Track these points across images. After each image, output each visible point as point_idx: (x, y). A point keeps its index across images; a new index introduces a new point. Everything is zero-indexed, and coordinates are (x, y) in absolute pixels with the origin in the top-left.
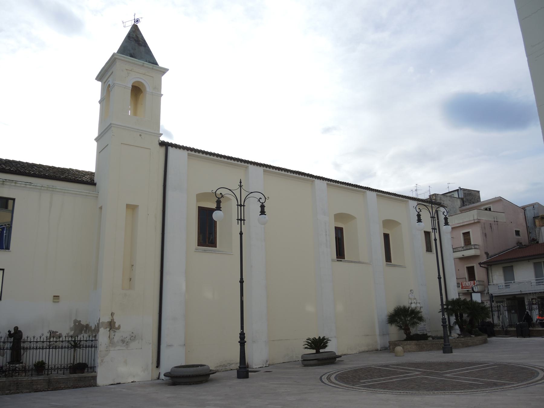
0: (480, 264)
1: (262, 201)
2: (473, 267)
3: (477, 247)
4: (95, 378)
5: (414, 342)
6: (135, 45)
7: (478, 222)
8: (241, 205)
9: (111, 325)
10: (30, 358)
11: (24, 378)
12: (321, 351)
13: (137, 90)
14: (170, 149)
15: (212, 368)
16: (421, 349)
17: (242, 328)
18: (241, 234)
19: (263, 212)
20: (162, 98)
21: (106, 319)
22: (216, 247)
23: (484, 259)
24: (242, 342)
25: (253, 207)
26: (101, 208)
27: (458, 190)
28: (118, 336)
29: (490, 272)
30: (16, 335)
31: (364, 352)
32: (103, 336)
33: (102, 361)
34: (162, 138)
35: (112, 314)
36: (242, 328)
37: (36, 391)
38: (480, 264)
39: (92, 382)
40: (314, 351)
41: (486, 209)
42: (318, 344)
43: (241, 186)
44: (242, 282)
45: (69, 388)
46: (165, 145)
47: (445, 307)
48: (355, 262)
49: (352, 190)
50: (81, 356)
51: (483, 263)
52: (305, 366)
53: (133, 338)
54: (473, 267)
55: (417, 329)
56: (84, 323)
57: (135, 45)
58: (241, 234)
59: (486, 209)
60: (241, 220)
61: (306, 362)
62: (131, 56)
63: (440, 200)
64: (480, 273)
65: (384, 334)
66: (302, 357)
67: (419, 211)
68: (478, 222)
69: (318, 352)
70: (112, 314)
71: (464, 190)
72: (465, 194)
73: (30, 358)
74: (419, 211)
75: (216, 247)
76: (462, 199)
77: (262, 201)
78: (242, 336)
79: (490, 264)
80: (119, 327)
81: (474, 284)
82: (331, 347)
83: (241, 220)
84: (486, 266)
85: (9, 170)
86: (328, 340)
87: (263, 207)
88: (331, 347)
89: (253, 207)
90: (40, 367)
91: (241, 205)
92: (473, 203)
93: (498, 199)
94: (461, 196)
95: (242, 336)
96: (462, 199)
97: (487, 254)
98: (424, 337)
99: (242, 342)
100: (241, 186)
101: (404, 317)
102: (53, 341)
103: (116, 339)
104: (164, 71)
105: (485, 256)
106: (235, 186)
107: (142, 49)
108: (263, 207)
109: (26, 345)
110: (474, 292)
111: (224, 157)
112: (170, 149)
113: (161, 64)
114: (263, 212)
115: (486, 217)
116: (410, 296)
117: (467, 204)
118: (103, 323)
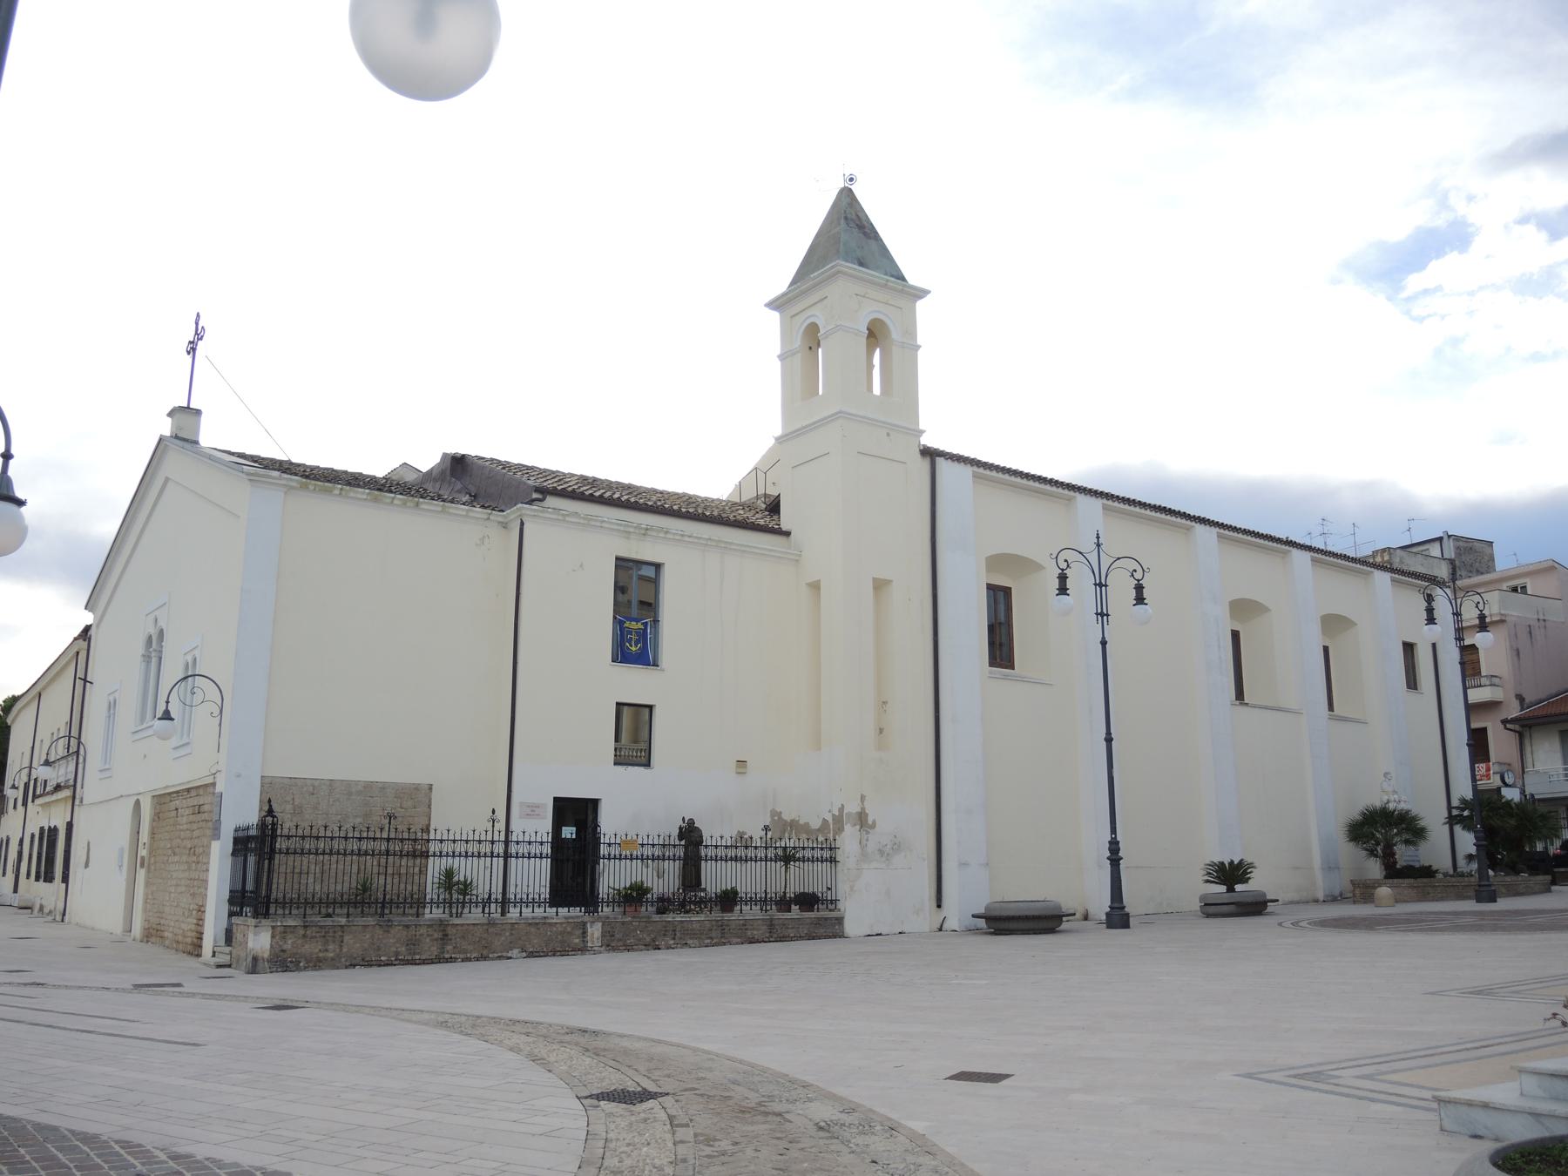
0: (1505, 722)
1: (1138, 575)
2: (1485, 730)
3: (1496, 681)
4: (840, 920)
5: (1407, 881)
6: (849, 238)
7: (1502, 621)
8: (1101, 585)
9: (862, 819)
10: (715, 877)
11: (698, 918)
12: (1238, 887)
13: (875, 334)
14: (940, 461)
15: (1065, 910)
16: (1424, 897)
17: (1113, 830)
18: (1104, 643)
19: (1140, 600)
20: (920, 353)
21: (853, 808)
22: (1013, 668)
23: (1514, 711)
24: (1115, 860)
25: (1120, 589)
26: (815, 587)
27: (1440, 539)
28: (874, 840)
29: (1527, 742)
30: (690, 834)
31: (1291, 903)
32: (848, 842)
33: (852, 888)
34: (927, 440)
35: (863, 798)
36: (1113, 830)
37: (752, 941)
38: (1505, 722)
39: (832, 929)
40: (1223, 888)
41: (1515, 590)
42: (1231, 874)
43: (1098, 545)
44: (1109, 740)
45: (801, 938)
46: (930, 454)
47: (1455, 812)
48: (1272, 709)
49: (1272, 549)
50: (799, 879)
51: (1513, 721)
52: (1208, 916)
53: (897, 847)
54: (1485, 730)
55: (1404, 855)
56: (787, 817)
57: (849, 238)
58: (1104, 643)
59: (1515, 590)
60: (1102, 614)
61: (1211, 909)
62: (861, 264)
63: (1401, 562)
64: (1501, 743)
65: (1330, 867)
66: (1202, 898)
67: (1064, 565)
68: (1502, 621)
69: (1231, 889)
70: (863, 798)
71: (1457, 538)
72: (1458, 548)
73: (715, 877)
74: (1064, 565)
75: (1013, 668)
76: (1452, 562)
77: (1138, 575)
78: (1114, 847)
79: (1526, 726)
80: (873, 826)
81: (1488, 769)
82: (1258, 883)
83: (1102, 614)
84: (1517, 727)
85: (601, 496)
86: (1251, 865)
87: (1139, 588)
88: (1258, 883)
89: (1120, 589)
90: (728, 899)
91: (1101, 585)
92: (1479, 572)
93: (1545, 565)
94: (1450, 552)
95: (1114, 847)
96: (1452, 562)
97: (1520, 698)
98: (1427, 872)
99: (1115, 860)
100: (1098, 545)
101: (1381, 830)
102: (740, 850)
103: (872, 846)
104: (921, 293)
105: (1515, 704)
106: (1088, 545)
107: (872, 243)
108: (1139, 588)
109: (711, 852)
110: (1506, 785)
111: (1028, 476)
112: (940, 461)
113: (913, 278)
114: (1140, 600)
115: (1517, 609)
116: (1385, 786)
117: (1464, 573)
118: (849, 814)
